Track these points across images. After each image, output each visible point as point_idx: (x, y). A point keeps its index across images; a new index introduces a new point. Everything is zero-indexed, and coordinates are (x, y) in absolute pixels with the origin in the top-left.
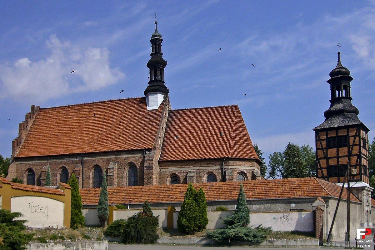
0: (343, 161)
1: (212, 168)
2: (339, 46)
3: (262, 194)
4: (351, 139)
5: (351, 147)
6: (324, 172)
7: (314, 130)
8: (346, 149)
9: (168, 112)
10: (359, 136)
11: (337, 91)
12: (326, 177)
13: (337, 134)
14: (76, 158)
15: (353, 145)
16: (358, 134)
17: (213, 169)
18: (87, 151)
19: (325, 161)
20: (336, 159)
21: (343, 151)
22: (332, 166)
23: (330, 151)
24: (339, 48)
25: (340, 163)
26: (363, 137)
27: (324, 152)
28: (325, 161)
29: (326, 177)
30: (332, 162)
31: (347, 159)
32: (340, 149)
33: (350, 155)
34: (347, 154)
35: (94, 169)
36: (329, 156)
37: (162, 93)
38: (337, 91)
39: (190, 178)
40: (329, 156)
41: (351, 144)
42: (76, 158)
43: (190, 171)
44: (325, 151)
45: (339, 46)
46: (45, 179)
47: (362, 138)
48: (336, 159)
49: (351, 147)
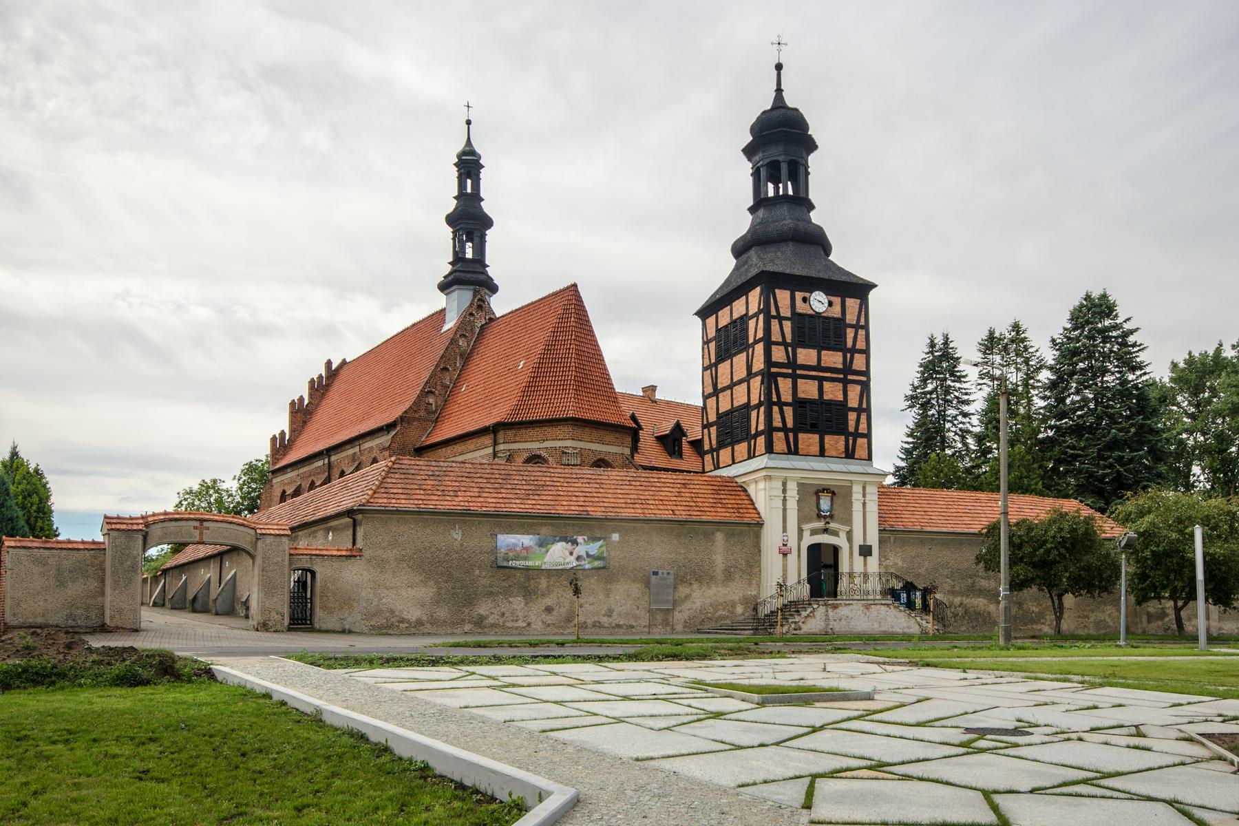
7: (696, 314)
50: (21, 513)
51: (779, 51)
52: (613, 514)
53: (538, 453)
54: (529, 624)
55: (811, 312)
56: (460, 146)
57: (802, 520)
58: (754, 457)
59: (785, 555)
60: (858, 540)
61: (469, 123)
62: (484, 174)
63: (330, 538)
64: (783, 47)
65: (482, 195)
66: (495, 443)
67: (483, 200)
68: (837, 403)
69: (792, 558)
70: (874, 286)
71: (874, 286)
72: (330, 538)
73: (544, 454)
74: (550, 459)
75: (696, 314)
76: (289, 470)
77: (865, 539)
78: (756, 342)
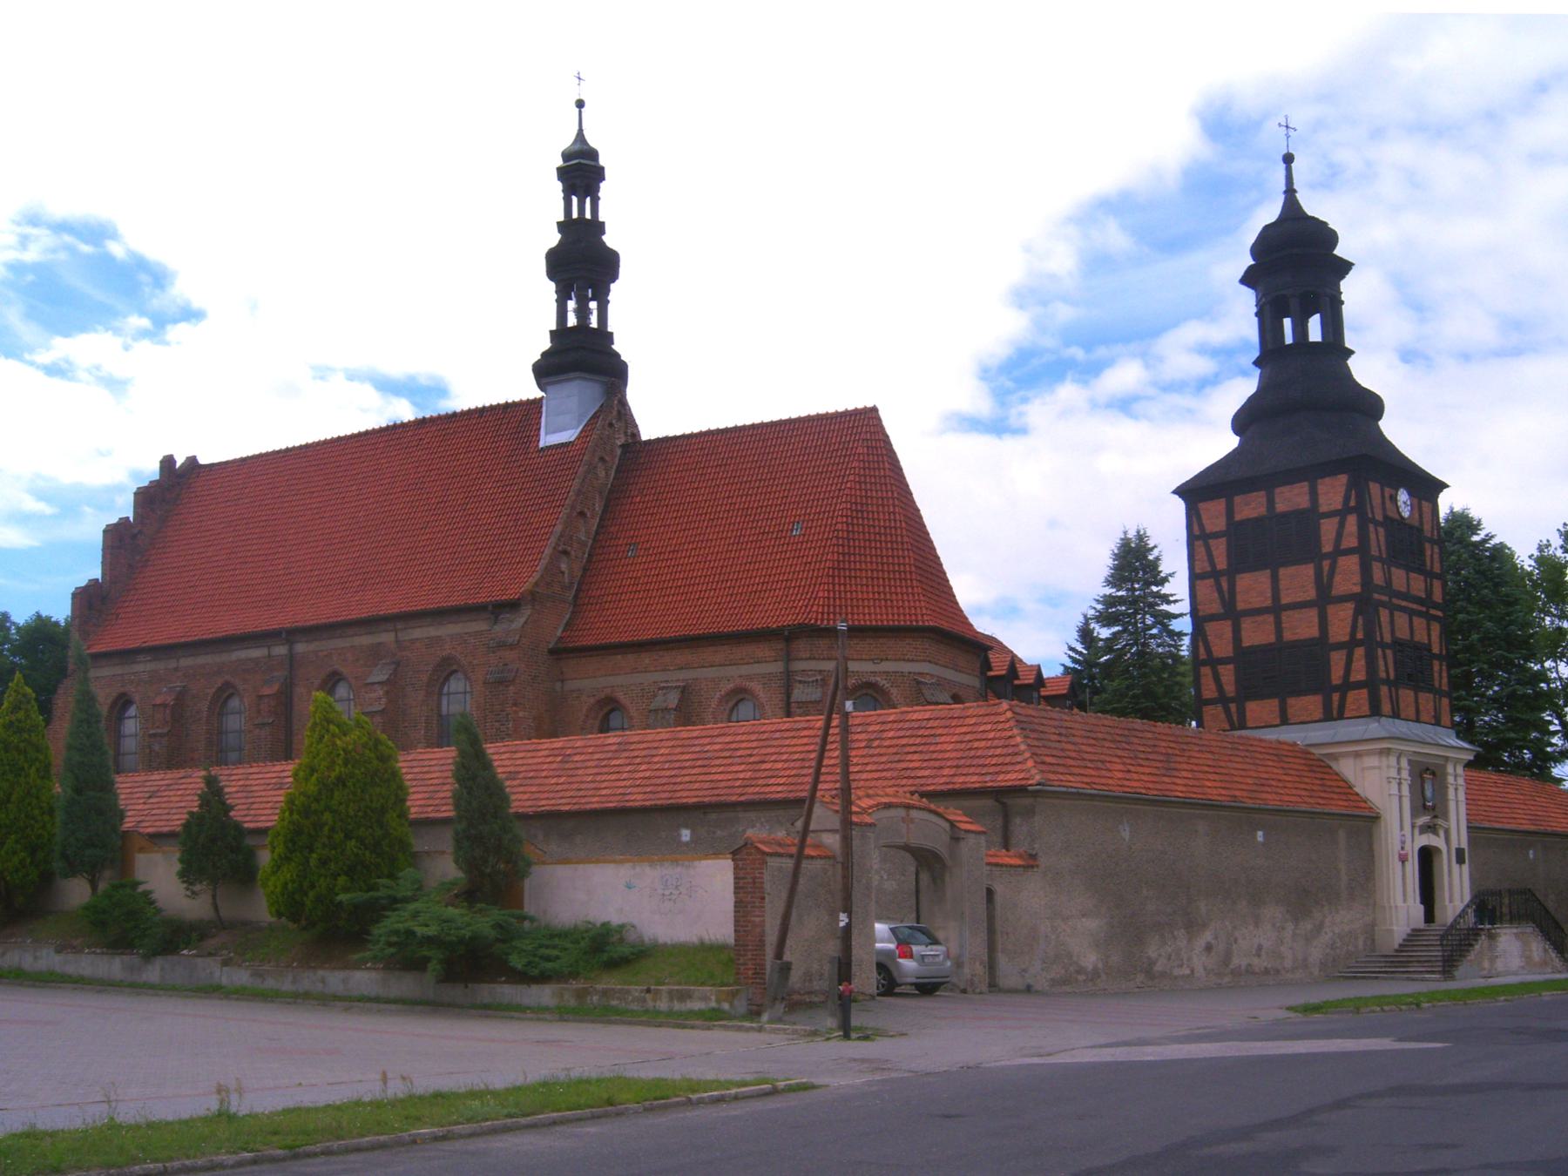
0: (1302, 626)
1: (745, 670)
2: (1287, 127)
3: (782, 781)
4: (1328, 528)
5: (1326, 564)
6: (1224, 679)
7: (1176, 492)
8: (1308, 570)
9: (619, 451)
10: (1360, 509)
11: (1372, 485)
12: (1232, 700)
13: (1271, 502)
14: (269, 647)
15: (1339, 552)
16: (1352, 503)
17: (750, 678)
18: (310, 617)
19: (1226, 628)
20: (1270, 618)
21: (1298, 581)
22: (1253, 650)
23: (1244, 581)
24: (1288, 137)
25: (1288, 636)
26: (1386, 517)
27: (1220, 590)
28: (1226, 628)
29: (1232, 700)
30: (1257, 634)
31: (1312, 614)
32: (1282, 571)
33: (1324, 598)
34: (1311, 594)
35: (1555, 763)
36: (1240, 606)
37: (583, 375)
38: (1372, 485)
39: (660, 714)
40: (1240, 606)
41: (1327, 548)
42: (269, 647)
43: (664, 688)
44: (1225, 585)
45: (1287, 127)
46: (162, 735)
47: (1379, 517)
48: (1270, 618)
49: (1326, 564)
50: (372, 755)
51: (1288, 137)
52: (975, 778)
53: (873, 679)
54: (1192, 971)
55: (1397, 517)
56: (567, 140)
57: (1414, 815)
58: (1341, 717)
59: (1403, 862)
60: (1454, 845)
61: (580, 104)
62: (605, 189)
63: (1531, 856)
64: (1291, 132)
65: (1349, 343)
66: (789, 658)
67: (1351, 352)
68: (1310, 642)
69: (1408, 865)
70: (1447, 486)
71: (1447, 486)
72: (1531, 856)
73: (882, 682)
74: (894, 691)
75: (1176, 492)
76: (141, 658)
77: (1459, 844)
78: (1339, 552)
